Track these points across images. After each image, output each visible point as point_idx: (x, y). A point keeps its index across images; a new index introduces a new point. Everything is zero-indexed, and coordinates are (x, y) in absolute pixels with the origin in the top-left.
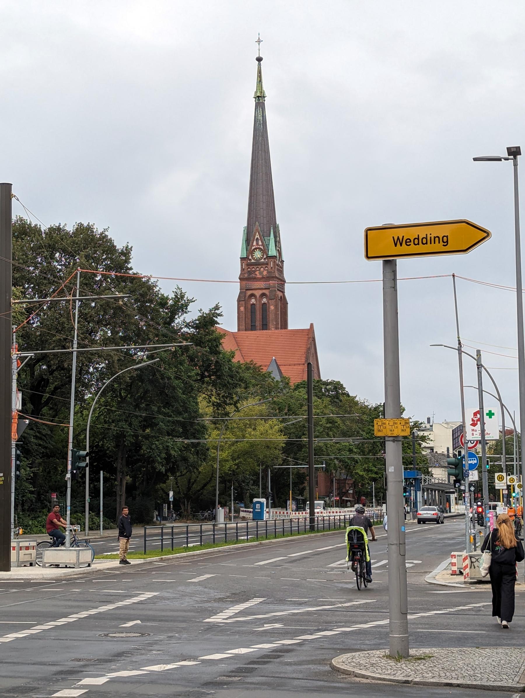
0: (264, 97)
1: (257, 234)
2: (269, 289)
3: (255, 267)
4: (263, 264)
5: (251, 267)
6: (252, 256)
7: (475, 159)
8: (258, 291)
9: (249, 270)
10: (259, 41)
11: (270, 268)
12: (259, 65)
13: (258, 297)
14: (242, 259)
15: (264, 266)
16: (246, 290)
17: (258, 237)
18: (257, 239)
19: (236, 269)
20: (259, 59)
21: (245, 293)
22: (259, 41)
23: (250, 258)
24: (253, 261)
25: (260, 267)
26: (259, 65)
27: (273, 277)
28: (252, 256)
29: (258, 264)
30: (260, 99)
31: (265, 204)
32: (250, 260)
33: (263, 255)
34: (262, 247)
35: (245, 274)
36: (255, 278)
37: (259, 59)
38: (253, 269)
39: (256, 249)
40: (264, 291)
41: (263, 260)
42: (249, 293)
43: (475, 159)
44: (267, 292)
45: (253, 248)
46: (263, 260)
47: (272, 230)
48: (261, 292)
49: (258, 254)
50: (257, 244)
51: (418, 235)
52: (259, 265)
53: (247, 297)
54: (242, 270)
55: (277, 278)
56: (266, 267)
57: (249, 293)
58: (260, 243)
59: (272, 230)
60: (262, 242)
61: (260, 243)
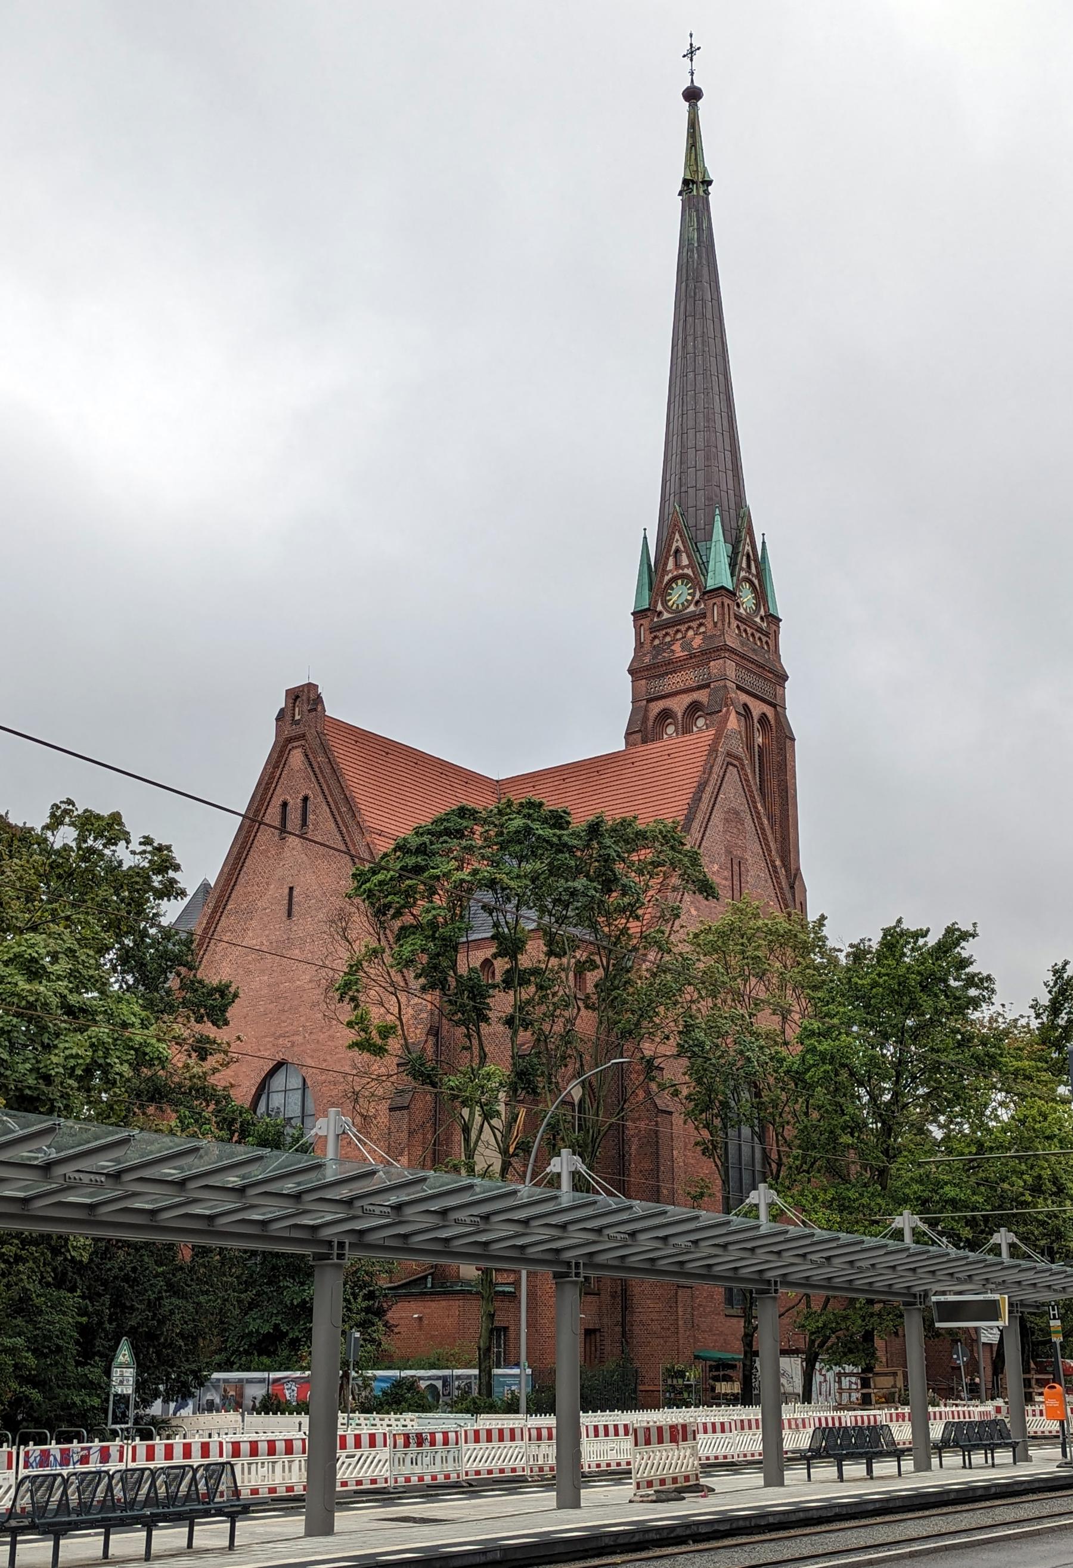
0: (710, 183)
1: (677, 536)
2: (708, 686)
3: (671, 631)
4: (693, 617)
5: (660, 634)
6: (665, 603)
7: (290, 914)
8: (678, 698)
9: (657, 642)
10: (691, 52)
11: (710, 625)
13: (680, 715)
14: (638, 615)
15: (694, 624)
16: (649, 701)
17: (680, 544)
18: (677, 551)
19: (621, 642)
20: (692, 95)
21: (646, 710)
22: (691, 52)
23: (660, 608)
24: (666, 615)
25: (683, 628)
27: (718, 649)
28: (665, 603)
29: (680, 620)
30: (695, 187)
31: (701, 454)
32: (660, 614)
33: (693, 595)
34: (689, 572)
35: (645, 655)
36: (670, 662)
37: (692, 95)
38: (668, 639)
39: (674, 579)
40: (696, 696)
41: (692, 608)
42: (656, 707)
43: (290, 914)
44: (702, 696)
45: (667, 578)
46: (692, 608)
47: (718, 518)
48: (687, 699)
49: (680, 594)
50: (677, 565)
51: (1066, 963)
52: (681, 622)
53: (650, 723)
54: (639, 645)
55: (733, 651)
56: (701, 625)
57: (656, 707)
58: (685, 561)
59: (718, 518)
60: (688, 557)
61: (685, 561)
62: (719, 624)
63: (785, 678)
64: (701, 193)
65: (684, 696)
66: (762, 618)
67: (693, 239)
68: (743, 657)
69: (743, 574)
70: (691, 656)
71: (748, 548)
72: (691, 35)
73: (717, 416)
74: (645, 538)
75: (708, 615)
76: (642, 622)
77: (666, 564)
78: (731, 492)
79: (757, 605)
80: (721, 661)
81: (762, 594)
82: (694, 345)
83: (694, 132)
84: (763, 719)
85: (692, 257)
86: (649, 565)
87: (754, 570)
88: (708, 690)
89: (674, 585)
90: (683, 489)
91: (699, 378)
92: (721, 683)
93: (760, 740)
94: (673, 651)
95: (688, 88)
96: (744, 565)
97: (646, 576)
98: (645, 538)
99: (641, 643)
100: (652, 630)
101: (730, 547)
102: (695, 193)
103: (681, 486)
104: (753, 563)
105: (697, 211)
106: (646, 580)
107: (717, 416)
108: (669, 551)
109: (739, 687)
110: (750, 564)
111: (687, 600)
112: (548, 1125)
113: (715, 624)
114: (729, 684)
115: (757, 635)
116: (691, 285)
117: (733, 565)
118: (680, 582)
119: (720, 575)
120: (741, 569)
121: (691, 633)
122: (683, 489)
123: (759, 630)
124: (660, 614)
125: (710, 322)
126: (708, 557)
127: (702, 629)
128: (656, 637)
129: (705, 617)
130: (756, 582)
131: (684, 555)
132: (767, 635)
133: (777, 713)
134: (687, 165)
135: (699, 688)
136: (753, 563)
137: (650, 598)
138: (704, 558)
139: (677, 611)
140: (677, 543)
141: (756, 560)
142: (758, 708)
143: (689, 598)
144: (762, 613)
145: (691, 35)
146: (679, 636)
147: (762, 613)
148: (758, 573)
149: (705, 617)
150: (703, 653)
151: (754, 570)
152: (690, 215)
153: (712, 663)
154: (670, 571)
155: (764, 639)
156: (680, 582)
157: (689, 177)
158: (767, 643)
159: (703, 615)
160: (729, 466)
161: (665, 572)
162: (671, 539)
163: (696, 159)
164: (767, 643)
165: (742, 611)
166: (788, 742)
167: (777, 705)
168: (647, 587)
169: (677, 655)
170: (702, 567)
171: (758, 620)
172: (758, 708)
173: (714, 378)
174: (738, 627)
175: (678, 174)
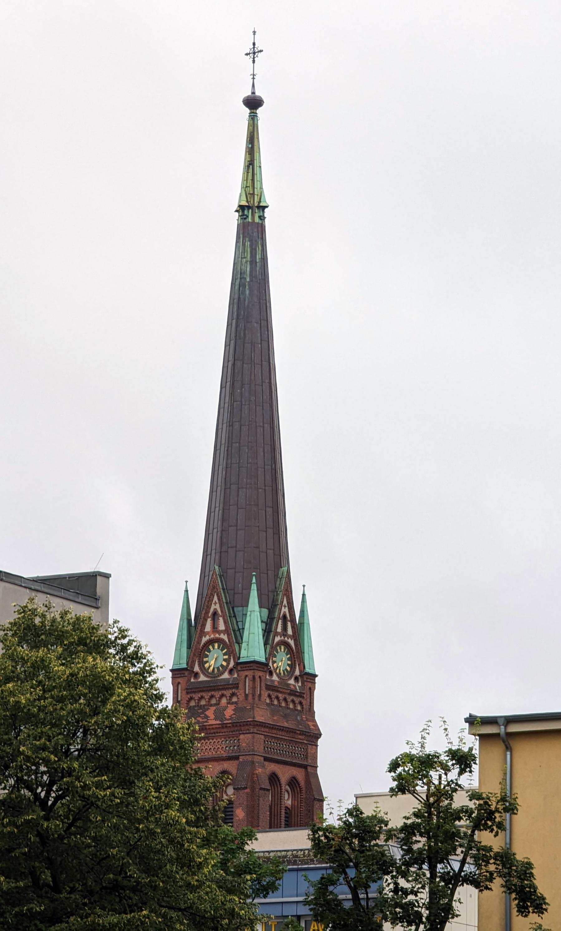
0: (264, 208)
1: (216, 599)
2: (237, 758)
3: (207, 695)
4: (226, 686)
5: (197, 696)
6: (202, 664)
9: (192, 703)
10: (254, 53)
11: (242, 697)
12: (253, 118)
15: (228, 693)
17: (218, 607)
18: (215, 613)
20: (253, 103)
22: (254, 53)
24: (202, 678)
25: (217, 694)
26: (253, 118)
27: (247, 724)
29: (214, 686)
32: (196, 675)
34: (225, 637)
37: (253, 103)
38: (203, 703)
39: (211, 642)
40: (226, 765)
41: (226, 676)
45: (204, 639)
46: (226, 676)
47: (254, 587)
49: (215, 659)
56: (233, 695)
59: (254, 587)
60: (225, 623)
61: (222, 627)
62: (250, 697)
63: (318, 735)
64: (257, 220)
65: (216, 764)
66: (296, 679)
67: (245, 273)
68: (272, 727)
69: (277, 639)
70: (224, 726)
71: (285, 610)
72: (254, 33)
73: (260, 471)
74: (187, 591)
75: (241, 686)
76: (179, 680)
77: (204, 625)
78: (271, 552)
79: (292, 666)
80: (249, 736)
81: (297, 655)
82: (241, 393)
83: (253, 147)
84: (293, 782)
85: (244, 293)
86: (189, 620)
87: (290, 632)
88: (236, 762)
89: (211, 647)
90: (224, 549)
91: (245, 429)
92: (249, 758)
93: (289, 802)
94: (207, 717)
95: (248, 97)
96: (279, 630)
97: (185, 632)
98: (187, 591)
99: (178, 702)
100: (189, 691)
101: (265, 612)
102: (250, 219)
103: (221, 545)
104: (289, 624)
105: (251, 241)
106: (185, 637)
107: (260, 471)
108: (207, 612)
109: (266, 759)
110: (288, 631)
111: (222, 666)
112: (265, 897)
113: (246, 696)
114: (257, 759)
115: (290, 698)
116: (241, 325)
117: (267, 632)
118: (216, 645)
119: (253, 648)
120: (276, 634)
121: (224, 701)
122: (224, 549)
123: (293, 693)
124: (196, 675)
125: (258, 367)
126: (244, 624)
127: (234, 699)
128: (191, 698)
129: (237, 688)
130: (292, 642)
131: (221, 619)
132: (301, 695)
133: (307, 775)
134: (245, 187)
135: (230, 758)
136: (289, 624)
137: (188, 658)
138: (240, 624)
139: (212, 675)
140: (215, 606)
141: (293, 620)
142: (285, 774)
143: (224, 664)
144: (297, 673)
145: (254, 33)
146: (213, 701)
147: (297, 673)
148: (294, 632)
149: (237, 688)
150: (234, 724)
151: (290, 632)
152: (244, 244)
153: (242, 737)
154: (208, 633)
155: (297, 700)
156: (216, 645)
157: (244, 203)
158: (301, 703)
159: (236, 686)
160: (270, 523)
161: (203, 633)
162: (210, 601)
163: (253, 180)
164: (301, 703)
165: (275, 678)
166: (316, 804)
167: (309, 766)
168: (185, 645)
169: (211, 722)
170: (237, 634)
171: (292, 682)
172: (285, 774)
173: (260, 430)
174: (269, 696)
175: (234, 196)
